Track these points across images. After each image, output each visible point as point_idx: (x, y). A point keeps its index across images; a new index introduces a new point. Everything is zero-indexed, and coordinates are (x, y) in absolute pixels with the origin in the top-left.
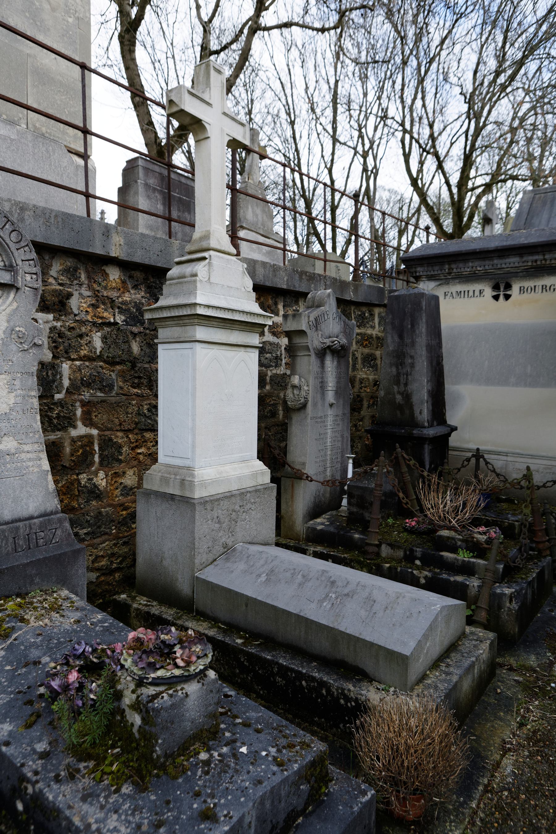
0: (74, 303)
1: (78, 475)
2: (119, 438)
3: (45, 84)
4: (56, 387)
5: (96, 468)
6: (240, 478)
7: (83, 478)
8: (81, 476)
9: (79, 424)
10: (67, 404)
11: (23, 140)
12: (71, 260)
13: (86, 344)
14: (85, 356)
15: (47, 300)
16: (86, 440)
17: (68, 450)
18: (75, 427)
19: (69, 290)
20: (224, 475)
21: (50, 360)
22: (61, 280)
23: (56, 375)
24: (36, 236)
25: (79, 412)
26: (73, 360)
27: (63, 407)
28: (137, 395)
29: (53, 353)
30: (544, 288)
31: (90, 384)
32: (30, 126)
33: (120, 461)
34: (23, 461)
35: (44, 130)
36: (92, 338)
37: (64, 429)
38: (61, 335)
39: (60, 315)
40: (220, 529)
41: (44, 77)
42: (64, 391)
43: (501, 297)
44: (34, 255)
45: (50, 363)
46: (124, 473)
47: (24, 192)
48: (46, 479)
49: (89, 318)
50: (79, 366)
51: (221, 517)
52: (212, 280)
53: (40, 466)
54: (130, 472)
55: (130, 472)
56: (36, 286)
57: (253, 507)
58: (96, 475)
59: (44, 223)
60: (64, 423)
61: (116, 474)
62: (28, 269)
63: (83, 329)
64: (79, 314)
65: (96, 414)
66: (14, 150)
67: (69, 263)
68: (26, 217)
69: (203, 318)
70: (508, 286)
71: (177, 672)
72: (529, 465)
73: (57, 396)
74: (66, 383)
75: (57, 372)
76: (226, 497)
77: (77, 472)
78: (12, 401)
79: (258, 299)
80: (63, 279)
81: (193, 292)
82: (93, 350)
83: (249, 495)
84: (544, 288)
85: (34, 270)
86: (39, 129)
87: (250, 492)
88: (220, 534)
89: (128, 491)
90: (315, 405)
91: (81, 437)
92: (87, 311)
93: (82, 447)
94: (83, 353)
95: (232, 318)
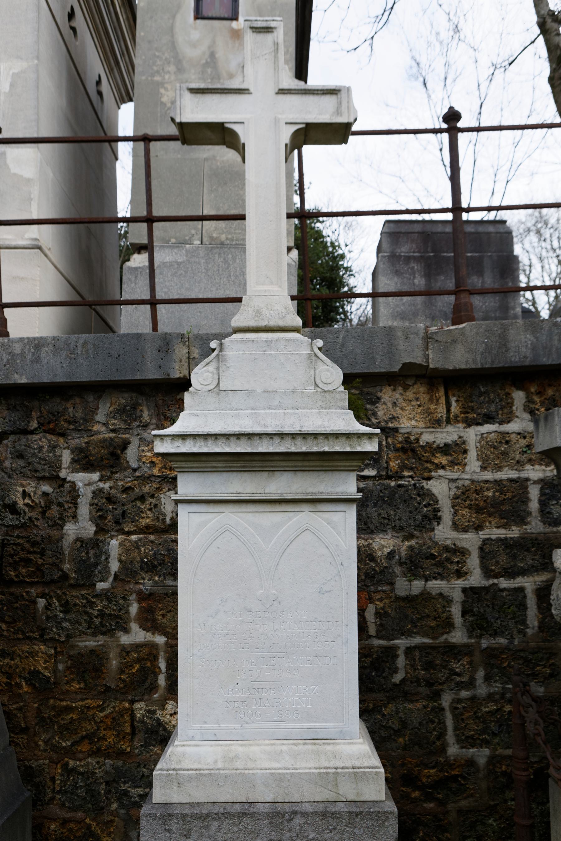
1: (132, 702)
3: (226, 184)
4: (100, 572)
5: (161, 696)
6: (280, 779)
7: (140, 708)
8: (137, 706)
9: (134, 626)
10: (116, 597)
11: (193, 260)
12: (126, 395)
13: (150, 510)
14: (147, 527)
15: (91, 455)
16: (146, 650)
17: (114, 664)
18: (127, 631)
19: (124, 436)
20: (239, 764)
21: (92, 536)
22: (113, 425)
23: (100, 556)
24: (56, 375)
25: (134, 609)
26: (129, 533)
27: (110, 601)
29: (97, 525)
31: (155, 567)
32: (205, 239)
36: (159, 499)
37: (110, 632)
38: (110, 499)
39: (112, 473)
42: (111, 579)
45: (91, 539)
47: (192, 320)
49: (156, 471)
50: (136, 542)
52: (222, 386)
58: (163, 708)
59: (67, 356)
60: (111, 625)
63: (146, 489)
64: (139, 467)
65: (163, 612)
66: (181, 275)
67: (123, 399)
68: (43, 355)
69: (182, 458)
73: (101, 586)
74: (114, 566)
75: (101, 552)
76: (228, 815)
77: (130, 697)
80: (115, 423)
82: (161, 517)
83: (298, 820)
86: (217, 238)
87: (303, 814)
91: (137, 647)
92: (152, 462)
93: (138, 660)
94: (144, 522)
95: (249, 450)
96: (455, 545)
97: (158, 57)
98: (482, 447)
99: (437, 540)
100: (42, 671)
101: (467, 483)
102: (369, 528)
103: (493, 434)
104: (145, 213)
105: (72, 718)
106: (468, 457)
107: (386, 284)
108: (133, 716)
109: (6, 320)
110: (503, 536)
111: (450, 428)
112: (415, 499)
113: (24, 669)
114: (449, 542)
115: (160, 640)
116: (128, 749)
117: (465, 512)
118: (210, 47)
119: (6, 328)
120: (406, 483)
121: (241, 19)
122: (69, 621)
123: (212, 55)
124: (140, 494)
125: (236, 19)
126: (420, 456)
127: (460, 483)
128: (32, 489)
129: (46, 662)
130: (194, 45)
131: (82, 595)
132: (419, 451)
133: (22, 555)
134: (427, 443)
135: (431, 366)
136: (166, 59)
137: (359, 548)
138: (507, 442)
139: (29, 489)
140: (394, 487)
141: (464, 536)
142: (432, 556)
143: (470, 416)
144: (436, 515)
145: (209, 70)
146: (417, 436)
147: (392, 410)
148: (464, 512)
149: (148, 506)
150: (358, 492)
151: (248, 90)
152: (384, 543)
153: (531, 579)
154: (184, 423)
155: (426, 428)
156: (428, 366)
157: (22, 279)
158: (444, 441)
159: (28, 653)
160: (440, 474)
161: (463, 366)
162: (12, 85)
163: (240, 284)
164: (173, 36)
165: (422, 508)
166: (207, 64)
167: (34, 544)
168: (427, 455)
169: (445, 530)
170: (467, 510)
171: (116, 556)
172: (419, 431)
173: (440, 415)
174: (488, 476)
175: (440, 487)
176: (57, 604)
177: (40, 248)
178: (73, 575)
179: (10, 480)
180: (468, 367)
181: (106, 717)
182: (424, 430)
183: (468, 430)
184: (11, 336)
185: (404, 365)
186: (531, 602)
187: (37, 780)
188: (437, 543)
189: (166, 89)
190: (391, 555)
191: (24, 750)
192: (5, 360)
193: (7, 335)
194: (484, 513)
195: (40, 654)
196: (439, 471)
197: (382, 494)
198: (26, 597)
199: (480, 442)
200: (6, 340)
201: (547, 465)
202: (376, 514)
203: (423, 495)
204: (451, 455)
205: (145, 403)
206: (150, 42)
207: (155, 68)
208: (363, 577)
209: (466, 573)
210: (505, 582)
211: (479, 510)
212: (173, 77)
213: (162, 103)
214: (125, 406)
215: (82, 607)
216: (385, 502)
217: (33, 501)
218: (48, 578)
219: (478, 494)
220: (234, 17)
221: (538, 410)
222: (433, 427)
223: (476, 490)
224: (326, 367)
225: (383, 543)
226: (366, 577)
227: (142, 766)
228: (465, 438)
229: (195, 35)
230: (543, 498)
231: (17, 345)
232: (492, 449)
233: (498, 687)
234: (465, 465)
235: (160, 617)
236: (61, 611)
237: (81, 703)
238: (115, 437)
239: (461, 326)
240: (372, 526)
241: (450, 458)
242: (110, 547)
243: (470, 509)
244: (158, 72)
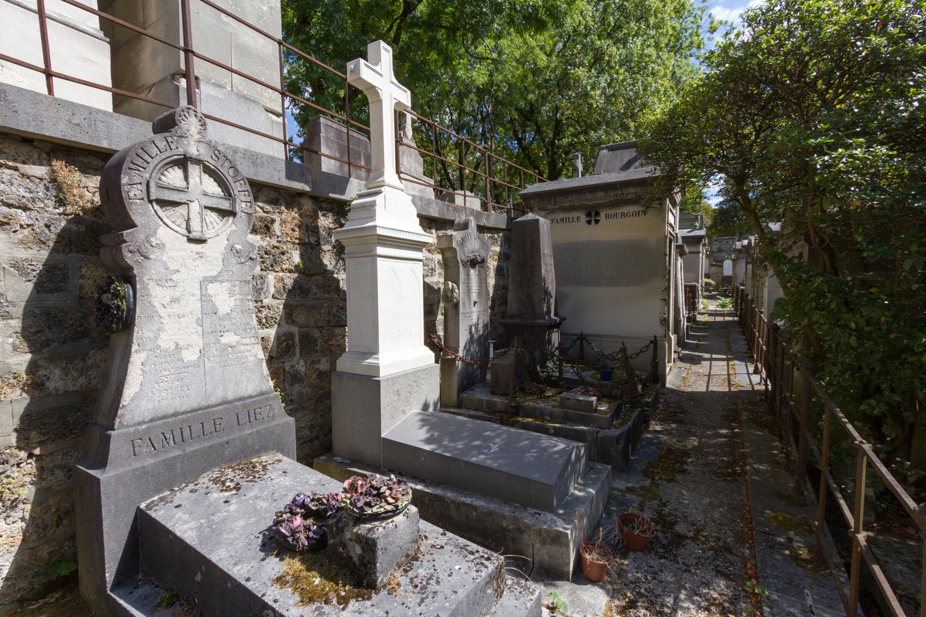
0: (276, 228)
2: (316, 333)
28: (327, 299)
30: (623, 214)
33: (316, 351)
34: (242, 352)
35: (245, 92)
41: (244, 51)
43: (593, 222)
44: (248, 188)
46: (319, 361)
48: (261, 366)
53: (256, 356)
54: (324, 360)
55: (324, 360)
56: (249, 212)
57: (423, 382)
61: (313, 363)
62: (244, 199)
70: (597, 214)
71: (389, 508)
72: (624, 340)
74: (272, 290)
78: (233, 303)
81: (372, 217)
84: (623, 214)
85: (248, 199)
89: (322, 375)
90: (464, 304)
93: (285, 340)
94: (284, 267)
108: (284, 369)
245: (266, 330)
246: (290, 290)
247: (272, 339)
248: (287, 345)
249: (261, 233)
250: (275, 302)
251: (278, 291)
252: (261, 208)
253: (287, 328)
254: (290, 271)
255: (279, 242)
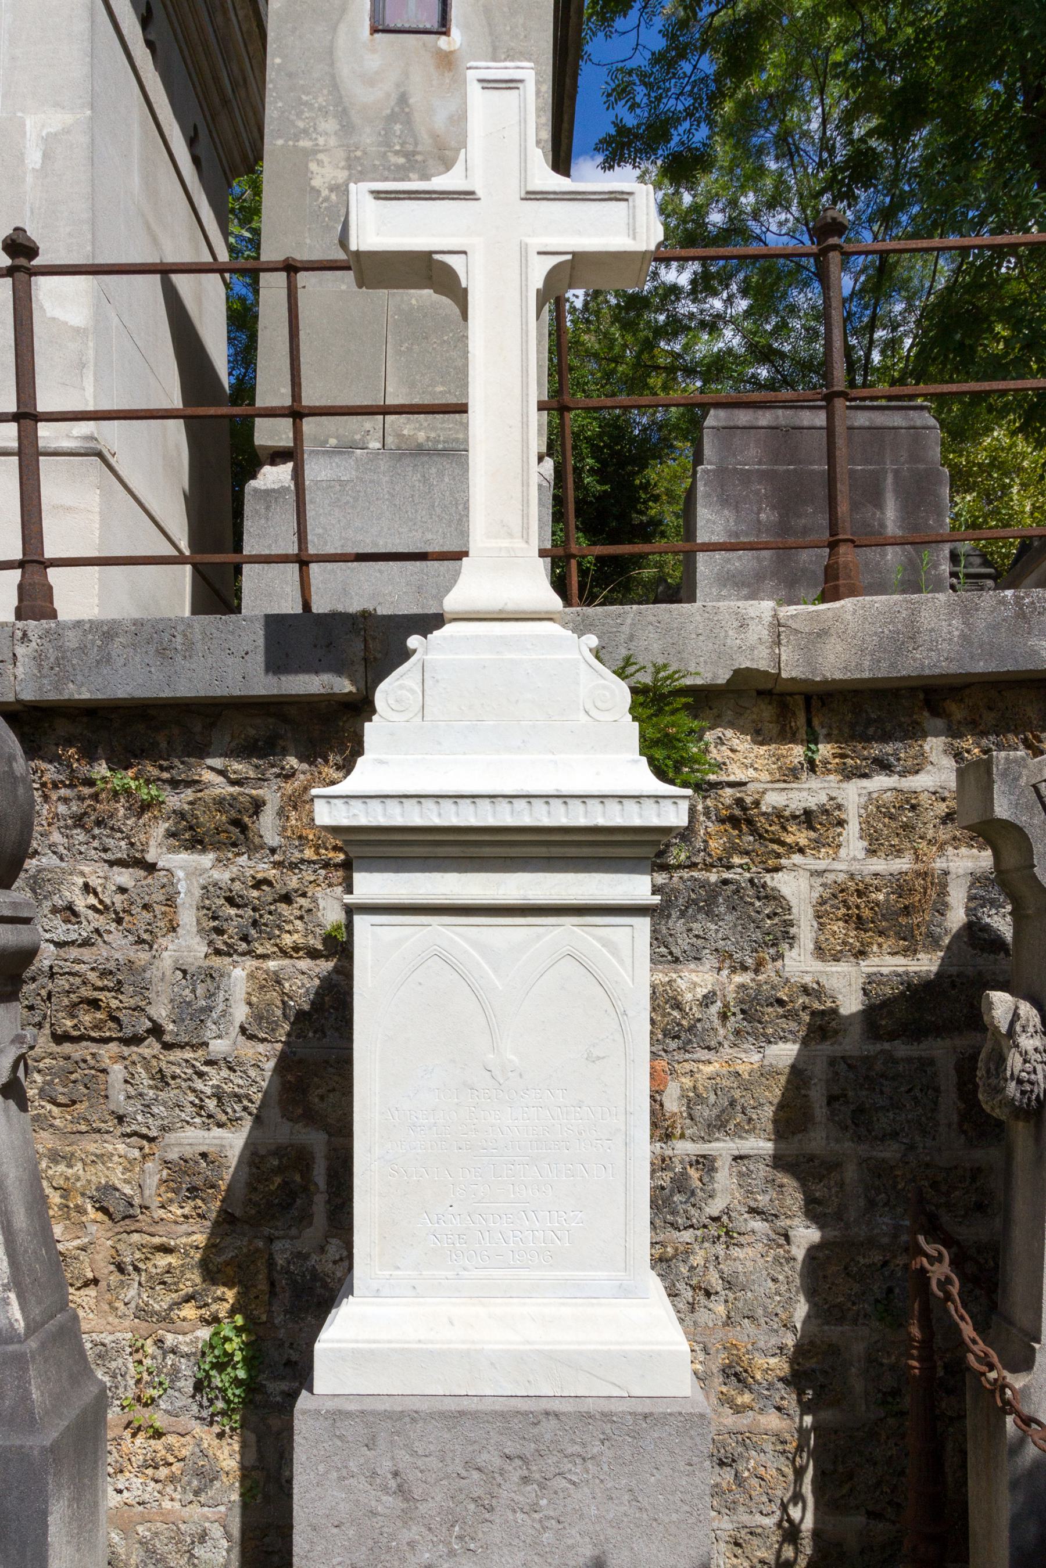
13: (301, 918)
19: (254, 792)
26: (264, 957)
32: (389, 440)
36: (315, 900)
40: (406, 1517)
50: (275, 973)
51: (412, 1476)
57: (577, 1472)
63: (293, 882)
66: (348, 502)
74: (240, 1013)
79: (648, 746)
88: (406, 1535)
93: (279, 1170)
94: (288, 940)
96: (818, 983)
97: (306, 104)
98: (868, 816)
99: (787, 975)
100: (119, 1186)
101: (841, 877)
102: (671, 953)
103: (889, 793)
104: (288, 402)
105: (170, 1264)
106: (845, 833)
107: (708, 521)
108: (271, 1264)
109: (51, 588)
110: (900, 970)
111: (814, 783)
112: (752, 904)
113: (89, 1182)
114: (807, 979)
115: (316, 1140)
116: (264, 1318)
117: (838, 927)
118: (398, 85)
119: (52, 603)
120: (737, 877)
121: (455, 31)
122: (164, 1104)
123: (403, 99)
124: (284, 892)
125: (446, 33)
126: (761, 831)
127: (830, 878)
128: (100, 881)
129: (126, 1170)
130: (370, 81)
131: (187, 1061)
132: (761, 822)
133: (86, 992)
134: (774, 808)
135: (784, 675)
136: (320, 109)
137: (654, 987)
138: (913, 808)
139: (94, 882)
140: (716, 884)
141: (834, 969)
142: (780, 1002)
143: (849, 761)
144: (787, 933)
145: (398, 127)
146: (757, 796)
147: (715, 751)
148: (835, 928)
149: (298, 913)
150: (653, 893)
151: (473, 193)
152: (696, 980)
153: (948, 1042)
154: (364, 776)
155: (772, 782)
156: (779, 674)
157: (69, 509)
158: (803, 805)
159: (96, 1156)
160: (796, 862)
161: (838, 676)
162: (46, 156)
163: (450, 521)
164: (332, 64)
165: (763, 920)
166: (392, 118)
167: (105, 973)
168: (773, 828)
169: (802, 958)
170: (841, 924)
171: (244, 996)
172: (760, 787)
173: (796, 761)
174: (879, 865)
175: (795, 886)
176: (144, 1075)
177: (100, 455)
178: (171, 1027)
179: (63, 864)
180: (848, 676)
181: (227, 1264)
182: (769, 786)
183: (844, 785)
184: (61, 617)
185: (737, 672)
186: (948, 1080)
187: (113, 1365)
188: (787, 980)
189: (320, 163)
190: (707, 1000)
191: (91, 1316)
192: (52, 660)
193: (53, 615)
194: (870, 929)
195: (116, 1158)
196: (793, 856)
197: (693, 896)
198: (92, 1062)
199: (866, 808)
200: (52, 624)
201: (981, 848)
202: (684, 928)
203: (766, 897)
204: (815, 830)
205: (289, 735)
206: (290, 75)
207: (301, 124)
208: (660, 1036)
209: (836, 1032)
210: (903, 1047)
211: (860, 923)
212: (333, 142)
213: (313, 188)
214: (257, 740)
215: (185, 1080)
216: (700, 909)
217: (101, 902)
218: (128, 1032)
219: (859, 897)
220: (443, 27)
221: (968, 751)
222: (785, 781)
223: (857, 890)
224: (603, 682)
225: (695, 979)
226: (665, 1036)
227: (287, 1345)
228: (839, 800)
229: (373, 62)
230: (972, 905)
231: (70, 634)
232: (886, 820)
233: (887, 1225)
234: (839, 846)
235: (317, 1100)
236: (151, 1087)
237: (184, 1240)
238: (239, 794)
239: (837, 604)
240: (677, 951)
241: (812, 835)
242: (232, 980)
243: (846, 922)
244: (305, 131)
245: (217, 1132)
246: (301, 1015)
247: (234, 1162)
248: (285, 1183)
249: (217, 846)
250: (250, 1051)
251: (259, 1017)
252: (221, 773)
253: (284, 1133)
254: (313, 954)
255: (277, 865)
